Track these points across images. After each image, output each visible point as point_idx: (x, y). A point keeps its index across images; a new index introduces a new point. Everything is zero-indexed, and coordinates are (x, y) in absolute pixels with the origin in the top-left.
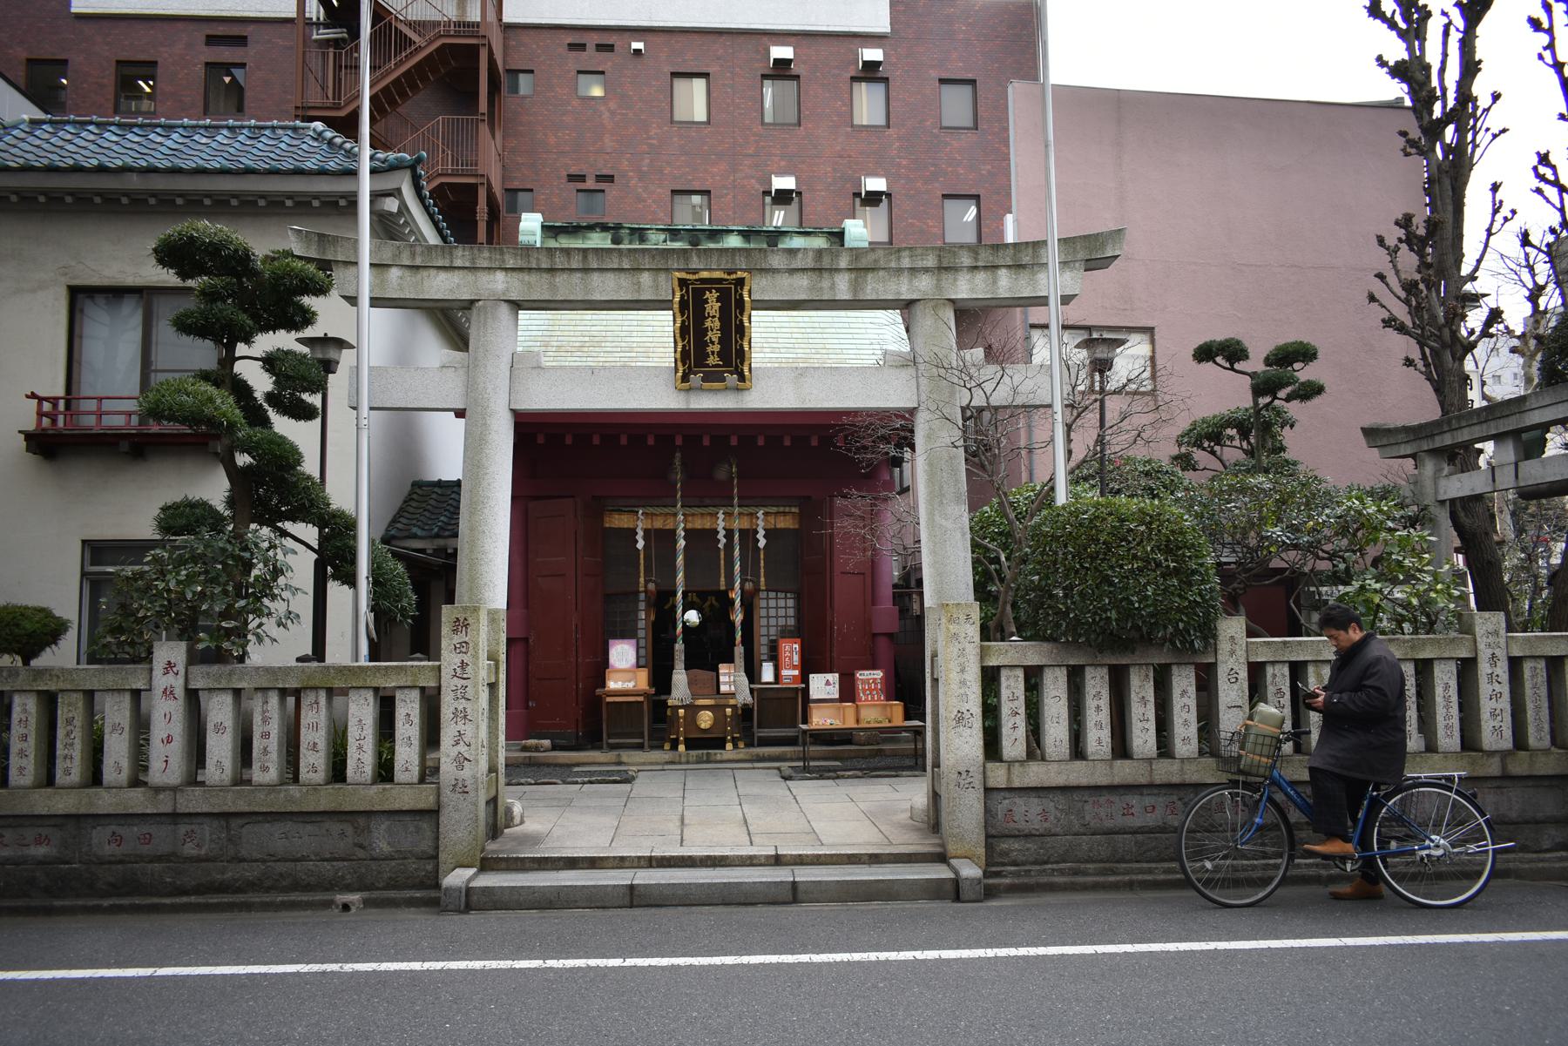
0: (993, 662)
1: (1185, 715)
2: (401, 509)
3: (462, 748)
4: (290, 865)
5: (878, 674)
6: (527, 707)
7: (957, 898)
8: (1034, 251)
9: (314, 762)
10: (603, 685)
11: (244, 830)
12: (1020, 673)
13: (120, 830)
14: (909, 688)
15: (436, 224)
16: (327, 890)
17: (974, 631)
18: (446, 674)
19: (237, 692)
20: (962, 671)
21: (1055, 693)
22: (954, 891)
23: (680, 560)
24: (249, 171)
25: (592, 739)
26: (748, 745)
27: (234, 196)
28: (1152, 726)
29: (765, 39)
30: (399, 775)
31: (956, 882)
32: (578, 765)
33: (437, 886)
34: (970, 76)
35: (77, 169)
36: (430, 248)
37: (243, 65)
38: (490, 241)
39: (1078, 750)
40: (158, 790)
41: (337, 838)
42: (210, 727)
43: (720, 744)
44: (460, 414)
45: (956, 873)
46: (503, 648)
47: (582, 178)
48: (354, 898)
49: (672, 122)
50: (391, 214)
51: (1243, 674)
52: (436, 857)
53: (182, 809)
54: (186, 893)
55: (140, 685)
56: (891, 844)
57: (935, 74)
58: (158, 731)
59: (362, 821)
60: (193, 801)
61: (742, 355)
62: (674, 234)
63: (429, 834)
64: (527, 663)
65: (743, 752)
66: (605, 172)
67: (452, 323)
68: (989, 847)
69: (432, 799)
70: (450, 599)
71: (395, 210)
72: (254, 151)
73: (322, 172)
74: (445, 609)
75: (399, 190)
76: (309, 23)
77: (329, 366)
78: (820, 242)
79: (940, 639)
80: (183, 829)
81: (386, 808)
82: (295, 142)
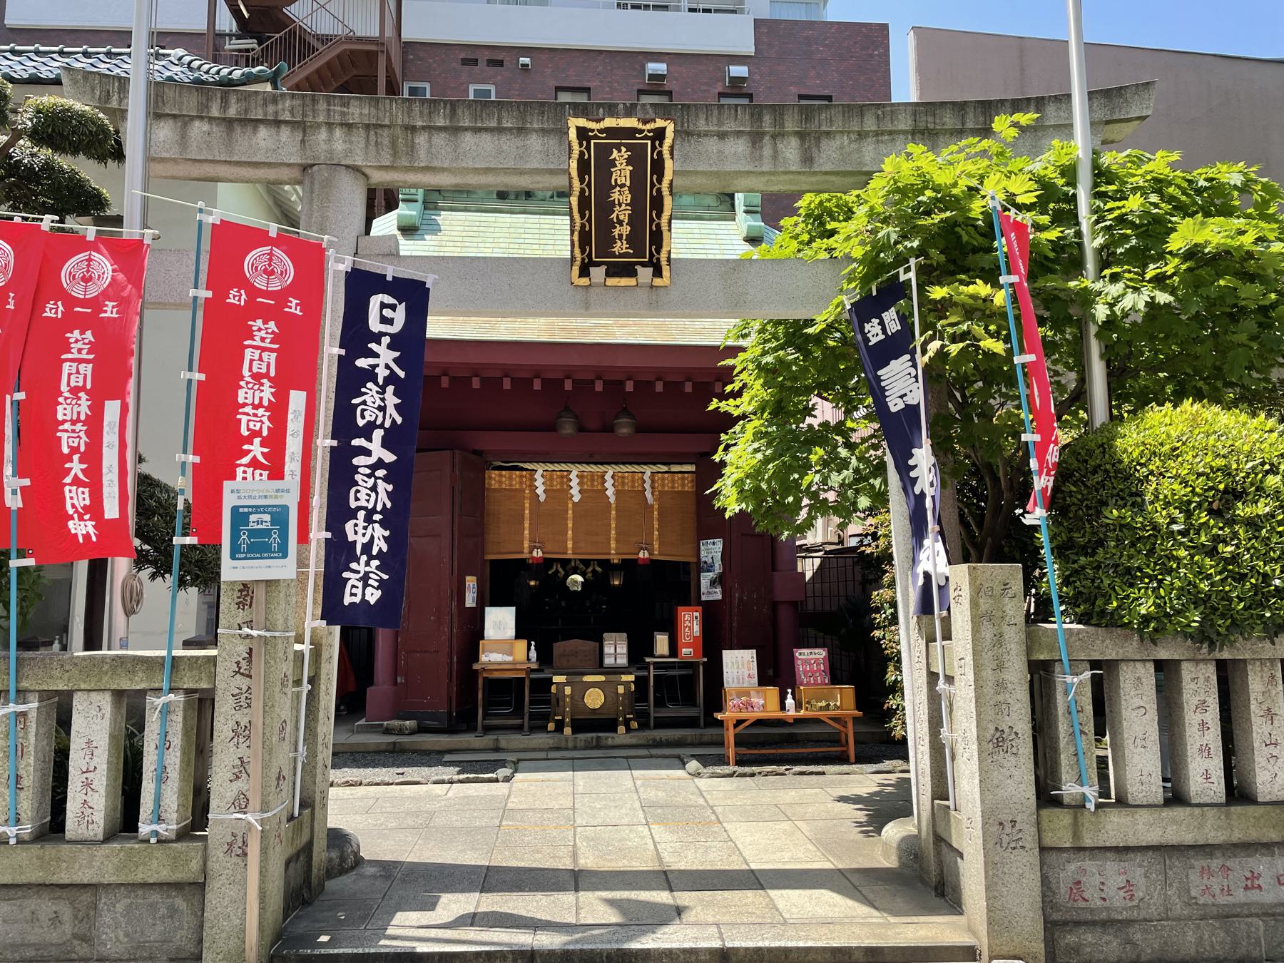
10: (477, 659)
14: (867, 670)
18: (224, 670)
25: (462, 721)
29: (640, 57)
32: (450, 752)
34: (826, 92)
43: (610, 726)
59: (86, 897)
63: (188, 921)
68: (1050, 943)
69: (195, 865)
76: (222, 35)
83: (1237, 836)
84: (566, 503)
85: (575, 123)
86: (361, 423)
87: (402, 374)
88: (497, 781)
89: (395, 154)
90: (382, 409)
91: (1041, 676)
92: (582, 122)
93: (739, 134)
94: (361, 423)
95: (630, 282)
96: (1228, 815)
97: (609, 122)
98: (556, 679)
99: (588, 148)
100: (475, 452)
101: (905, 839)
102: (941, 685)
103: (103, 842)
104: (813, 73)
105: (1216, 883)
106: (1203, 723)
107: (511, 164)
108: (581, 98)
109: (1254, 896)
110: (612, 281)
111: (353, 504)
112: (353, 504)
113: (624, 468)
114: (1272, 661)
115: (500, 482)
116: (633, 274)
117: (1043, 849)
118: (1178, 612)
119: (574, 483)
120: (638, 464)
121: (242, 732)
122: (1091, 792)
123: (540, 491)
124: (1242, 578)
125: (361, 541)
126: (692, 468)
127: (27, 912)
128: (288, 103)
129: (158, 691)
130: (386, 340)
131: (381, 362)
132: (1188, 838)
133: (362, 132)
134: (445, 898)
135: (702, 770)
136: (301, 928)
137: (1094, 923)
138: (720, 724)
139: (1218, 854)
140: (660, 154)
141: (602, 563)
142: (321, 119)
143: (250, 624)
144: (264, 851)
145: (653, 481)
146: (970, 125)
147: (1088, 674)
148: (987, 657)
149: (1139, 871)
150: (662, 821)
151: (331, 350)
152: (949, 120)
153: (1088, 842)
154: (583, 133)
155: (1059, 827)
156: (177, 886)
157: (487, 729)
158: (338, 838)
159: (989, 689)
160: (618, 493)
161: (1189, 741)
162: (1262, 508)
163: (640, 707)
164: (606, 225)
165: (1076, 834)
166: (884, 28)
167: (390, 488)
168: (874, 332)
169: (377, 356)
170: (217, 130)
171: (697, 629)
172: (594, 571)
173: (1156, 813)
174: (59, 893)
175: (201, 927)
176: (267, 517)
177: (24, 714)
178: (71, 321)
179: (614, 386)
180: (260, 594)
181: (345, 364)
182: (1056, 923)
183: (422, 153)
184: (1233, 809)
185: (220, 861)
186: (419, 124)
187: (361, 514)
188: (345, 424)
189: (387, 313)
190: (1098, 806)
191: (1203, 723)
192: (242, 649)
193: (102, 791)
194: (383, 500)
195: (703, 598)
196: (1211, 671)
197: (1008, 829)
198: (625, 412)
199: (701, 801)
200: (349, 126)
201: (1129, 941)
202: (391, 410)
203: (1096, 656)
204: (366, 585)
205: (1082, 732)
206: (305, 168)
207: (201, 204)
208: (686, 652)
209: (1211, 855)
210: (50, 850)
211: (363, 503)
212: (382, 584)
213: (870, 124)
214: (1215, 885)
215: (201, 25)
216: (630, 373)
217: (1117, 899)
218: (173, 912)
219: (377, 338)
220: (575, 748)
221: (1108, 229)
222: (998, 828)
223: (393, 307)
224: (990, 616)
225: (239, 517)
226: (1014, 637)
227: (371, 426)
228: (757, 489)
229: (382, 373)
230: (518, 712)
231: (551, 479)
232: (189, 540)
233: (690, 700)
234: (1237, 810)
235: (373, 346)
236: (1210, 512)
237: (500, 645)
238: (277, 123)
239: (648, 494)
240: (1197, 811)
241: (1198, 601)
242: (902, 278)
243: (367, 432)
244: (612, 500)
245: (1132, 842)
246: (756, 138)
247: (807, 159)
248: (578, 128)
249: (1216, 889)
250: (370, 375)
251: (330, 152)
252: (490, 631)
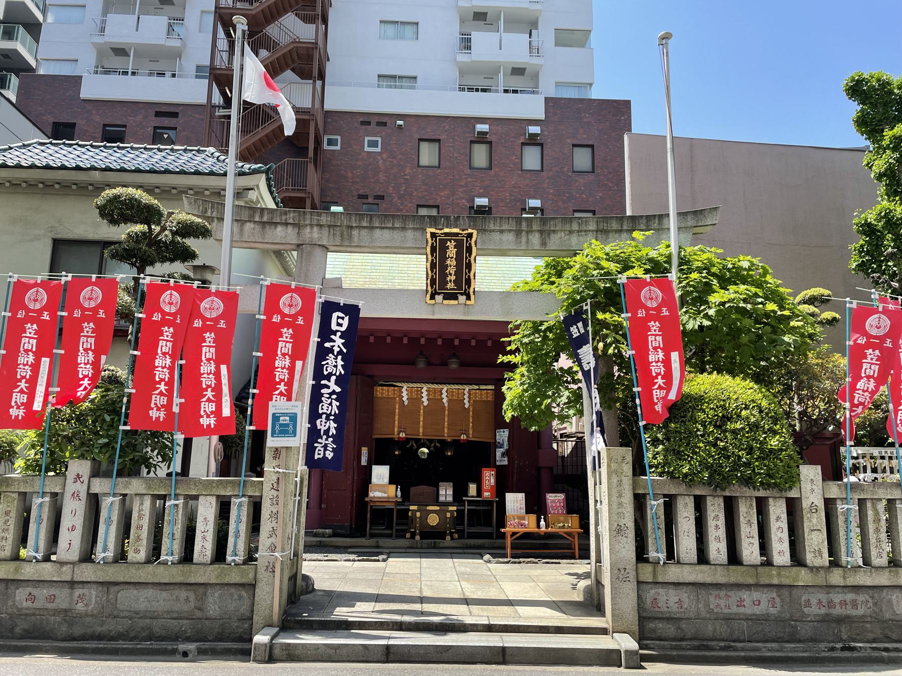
1: (780, 535)
5: (561, 496)
6: (320, 508)
8: (659, 220)
10: (367, 495)
13: (35, 592)
14: (578, 505)
16: (174, 640)
18: (267, 487)
21: (686, 514)
25: (358, 531)
27: (158, 187)
32: (351, 547)
34: (590, 143)
35: (63, 168)
36: (271, 211)
37: (175, 129)
39: (703, 558)
40: (62, 563)
47: (366, 197)
48: (192, 647)
49: (419, 166)
51: (821, 505)
52: (252, 619)
53: (77, 578)
54: (74, 639)
55: (57, 490)
57: (570, 141)
58: (66, 522)
59: (201, 590)
61: (468, 282)
63: (247, 602)
64: (322, 480)
66: (379, 193)
69: (251, 576)
73: (212, 173)
74: (87, 92)
75: (258, 186)
76: (214, 107)
80: (78, 592)
83: (732, 580)
84: (418, 404)
85: (430, 230)
86: (325, 373)
87: (345, 351)
88: (378, 561)
89: (342, 240)
90: (336, 366)
91: (640, 501)
92: (433, 230)
93: (510, 231)
94: (325, 373)
95: (455, 302)
96: (728, 570)
97: (447, 230)
98: (412, 508)
99: (436, 241)
100: (369, 376)
101: (587, 587)
102: (599, 504)
103: (211, 564)
104: (581, 131)
105: (722, 603)
106: (717, 526)
107: (398, 245)
108: (434, 212)
109: (742, 610)
110: (446, 302)
111: (320, 411)
112: (320, 411)
113: (453, 387)
114: (751, 497)
115: (382, 393)
116: (457, 299)
117: (639, 583)
118: (699, 472)
119: (425, 394)
120: (462, 384)
121: (275, 516)
122: (662, 556)
123: (405, 399)
124: (728, 457)
125: (323, 429)
126: (492, 387)
127: (174, 597)
128: (292, 215)
129: (236, 496)
130: (339, 334)
131: (336, 344)
132: (709, 580)
133: (327, 229)
134: (358, 604)
135: (492, 559)
136: (294, 611)
137: (663, 619)
138: (503, 536)
139: (724, 588)
140: (470, 244)
141: (439, 441)
142: (308, 222)
143: (278, 466)
144: (282, 570)
145: (470, 394)
146: (625, 228)
147: (662, 501)
148: (614, 491)
149: (686, 595)
150: (467, 580)
151: (314, 339)
152: (615, 225)
153: (660, 580)
154: (433, 235)
155: (647, 572)
156: (242, 585)
157: (372, 536)
158: (306, 578)
159: (615, 506)
160: (449, 401)
161: (710, 534)
162: (738, 426)
163: (461, 528)
164: (443, 275)
165: (655, 576)
166: (627, 103)
167: (338, 404)
168: (575, 331)
169: (334, 341)
170: (258, 228)
171: (493, 481)
172: (435, 446)
173: (693, 567)
174: (189, 587)
175: (253, 604)
176: (288, 418)
177: (177, 505)
178: (206, 328)
179: (448, 342)
180: (283, 452)
181: (320, 345)
182: (644, 618)
183: (356, 239)
184: (730, 567)
185: (263, 575)
186: (354, 225)
187: (324, 416)
188: (319, 374)
189: (340, 321)
190: (664, 563)
191: (717, 526)
192: (275, 478)
193: (211, 541)
194: (335, 410)
195: (498, 463)
196: (721, 501)
197: (622, 572)
198: (454, 355)
199: (489, 573)
200: (321, 226)
201: (680, 628)
202: (340, 367)
203: (666, 492)
204: (325, 450)
205: (659, 528)
206: (298, 245)
207: (262, 277)
208: (486, 494)
209: (720, 589)
210: (187, 567)
211: (325, 411)
212: (334, 450)
213: (575, 226)
214: (721, 603)
215: (203, 100)
216: (457, 335)
217: (674, 608)
218: (240, 597)
219: (335, 333)
220: (422, 548)
221: (684, 287)
222: (617, 569)
223: (343, 318)
224: (616, 472)
225: (276, 418)
226: (627, 481)
227: (330, 374)
228: (520, 405)
229: (336, 349)
230: (390, 527)
231: (411, 392)
232: (252, 428)
233: (489, 524)
234: (732, 567)
235: (333, 337)
236: (715, 426)
237: (381, 487)
238: (286, 224)
239: (466, 401)
240: (713, 567)
241: (707, 467)
242: (585, 308)
243: (328, 377)
244: (446, 405)
245: (681, 581)
246: (518, 233)
247: (544, 244)
248: (431, 233)
249: (723, 605)
250: (331, 350)
251: (311, 238)
252: (374, 480)
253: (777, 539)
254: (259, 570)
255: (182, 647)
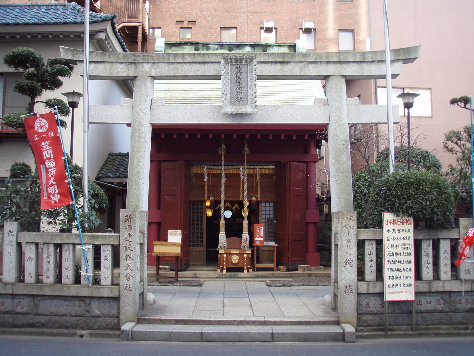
0: (361, 237)
1: (445, 261)
2: (104, 165)
3: (128, 271)
4: (58, 317)
7: (344, 340)
9: (68, 274)
11: (41, 302)
12: (374, 243)
15: (121, 43)
17: (354, 223)
19: (37, 244)
20: (348, 241)
22: (342, 337)
23: (223, 188)
24: (46, 24)
26: (253, 270)
28: (431, 266)
30: (103, 282)
31: (344, 334)
33: (119, 329)
38: (143, 50)
40: (6, 284)
41: (76, 308)
42: (26, 258)
43: (242, 270)
44: (129, 125)
45: (344, 330)
46: (146, 228)
47: (182, 22)
48: (85, 332)
50: (102, 39)
52: (118, 317)
53: (15, 292)
56: (316, 317)
59: (88, 301)
60: (20, 289)
62: (221, 45)
65: (251, 272)
67: (126, 86)
68: (358, 319)
70: (124, 207)
71: (104, 38)
72: (48, 15)
74: (122, 211)
75: (106, 30)
77: (74, 105)
78: (285, 50)
79: (339, 227)
80: (16, 301)
81: (97, 295)
82: (64, 11)
117: (358, 294)
175: (119, 309)
253: (444, 264)
254: (121, 289)
255: (79, 332)
